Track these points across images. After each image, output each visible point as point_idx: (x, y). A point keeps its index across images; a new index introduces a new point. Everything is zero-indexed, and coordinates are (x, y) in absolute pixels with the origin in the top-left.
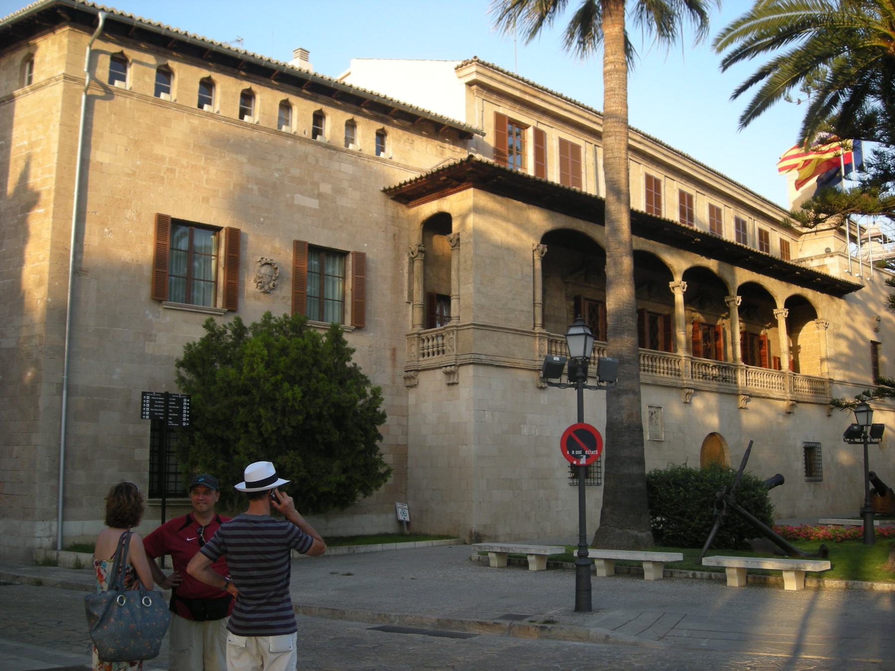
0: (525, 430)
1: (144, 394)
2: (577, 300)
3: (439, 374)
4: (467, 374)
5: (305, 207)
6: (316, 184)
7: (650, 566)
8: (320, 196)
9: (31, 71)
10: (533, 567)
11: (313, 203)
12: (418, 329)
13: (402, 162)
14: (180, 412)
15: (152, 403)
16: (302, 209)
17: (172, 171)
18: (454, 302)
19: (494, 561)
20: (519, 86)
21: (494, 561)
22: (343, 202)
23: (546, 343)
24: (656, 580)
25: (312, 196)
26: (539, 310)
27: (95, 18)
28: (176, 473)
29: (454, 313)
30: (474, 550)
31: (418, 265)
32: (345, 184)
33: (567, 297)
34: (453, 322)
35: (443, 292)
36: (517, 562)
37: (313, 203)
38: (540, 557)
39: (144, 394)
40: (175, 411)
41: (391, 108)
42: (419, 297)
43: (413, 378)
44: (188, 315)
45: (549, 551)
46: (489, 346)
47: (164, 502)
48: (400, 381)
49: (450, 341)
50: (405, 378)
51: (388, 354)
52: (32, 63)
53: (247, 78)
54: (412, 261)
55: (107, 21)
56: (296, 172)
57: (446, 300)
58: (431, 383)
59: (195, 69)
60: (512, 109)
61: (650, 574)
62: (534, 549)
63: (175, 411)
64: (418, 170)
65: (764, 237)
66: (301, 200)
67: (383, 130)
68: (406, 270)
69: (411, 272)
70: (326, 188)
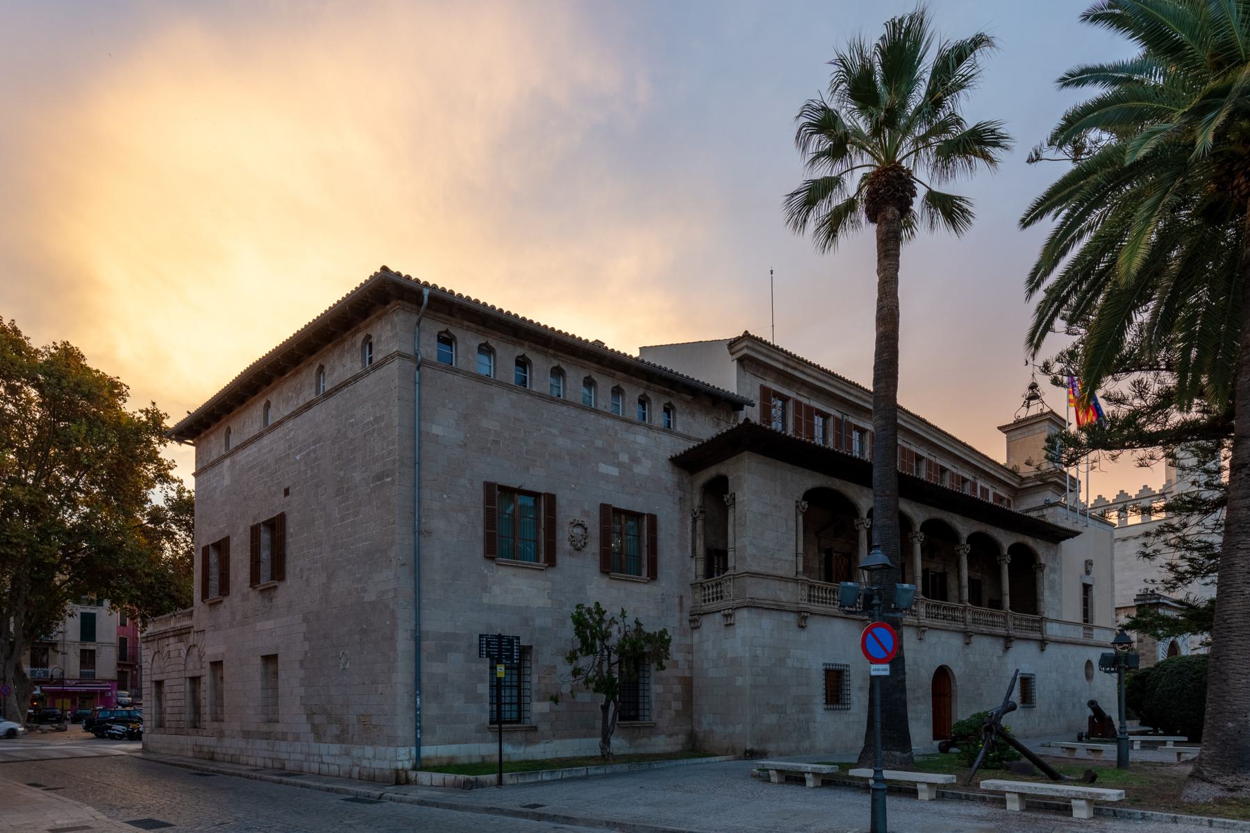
0: (789, 662)
1: (481, 636)
2: (829, 552)
3: (718, 617)
4: (743, 614)
5: (608, 475)
6: (616, 454)
7: (925, 787)
8: (619, 465)
9: (370, 352)
10: (810, 783)
11: (614, 471)
12: (700, 579)
13: (686, 433)
14: (512, 651)
15: (488, 643)
16: (605, 477)
17: (497, 442)
18: (730, 554)
19: (774, 779)
20: (782, 359)
21: (774, 779)
22: (637, 469)
23: (806, 588)
24: (931, 800)
25: (613, 465)
26: (801, 559)
27: (420, 294)
28: (511, 704)
29: (731, 564)
30: (755, 765)
31: (699, 523)
32: (640, 454)
33: (820, 550)
34: (730, 572)
35: (720, 547)
36: (794, 779)
37: (614, 471)
38: (816, 775)
39: (481, 636)
40: (507, 650)
41: (676, 382)
42: (701, 552)
43: (730, 615)
44: (516, 571)
45: (826, 769)
46: (758, 590)
47: (500, 728)
48: (686, 623)
49: (729, 589)
50: (690, 621)
51: (677, 600)
52: (371, 345)
53: (554, 356)
54: (695, 521)
55: (430, 297)
56: (599, 443)
57: (724, 554)
58: (711, 625)
59: (510, 347)
60: (776, 382)
61: (924, 795)
62: (810, 767)
63: (507, 650)
64: (698, 440)
65: (985, 492)
66: (605, 468)
67: (669, 404)
68: (690, 528)
69: (694, 530)
70: (624, 458)
